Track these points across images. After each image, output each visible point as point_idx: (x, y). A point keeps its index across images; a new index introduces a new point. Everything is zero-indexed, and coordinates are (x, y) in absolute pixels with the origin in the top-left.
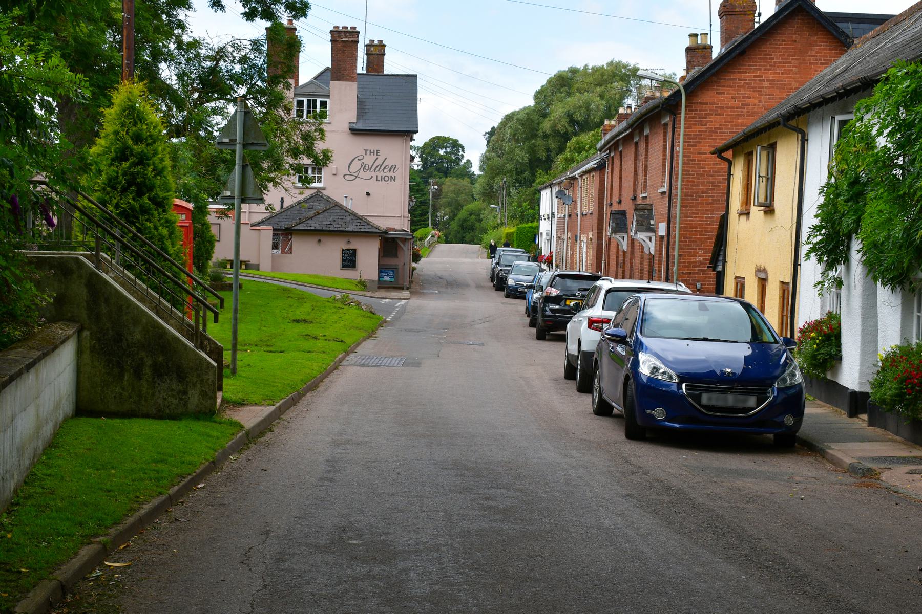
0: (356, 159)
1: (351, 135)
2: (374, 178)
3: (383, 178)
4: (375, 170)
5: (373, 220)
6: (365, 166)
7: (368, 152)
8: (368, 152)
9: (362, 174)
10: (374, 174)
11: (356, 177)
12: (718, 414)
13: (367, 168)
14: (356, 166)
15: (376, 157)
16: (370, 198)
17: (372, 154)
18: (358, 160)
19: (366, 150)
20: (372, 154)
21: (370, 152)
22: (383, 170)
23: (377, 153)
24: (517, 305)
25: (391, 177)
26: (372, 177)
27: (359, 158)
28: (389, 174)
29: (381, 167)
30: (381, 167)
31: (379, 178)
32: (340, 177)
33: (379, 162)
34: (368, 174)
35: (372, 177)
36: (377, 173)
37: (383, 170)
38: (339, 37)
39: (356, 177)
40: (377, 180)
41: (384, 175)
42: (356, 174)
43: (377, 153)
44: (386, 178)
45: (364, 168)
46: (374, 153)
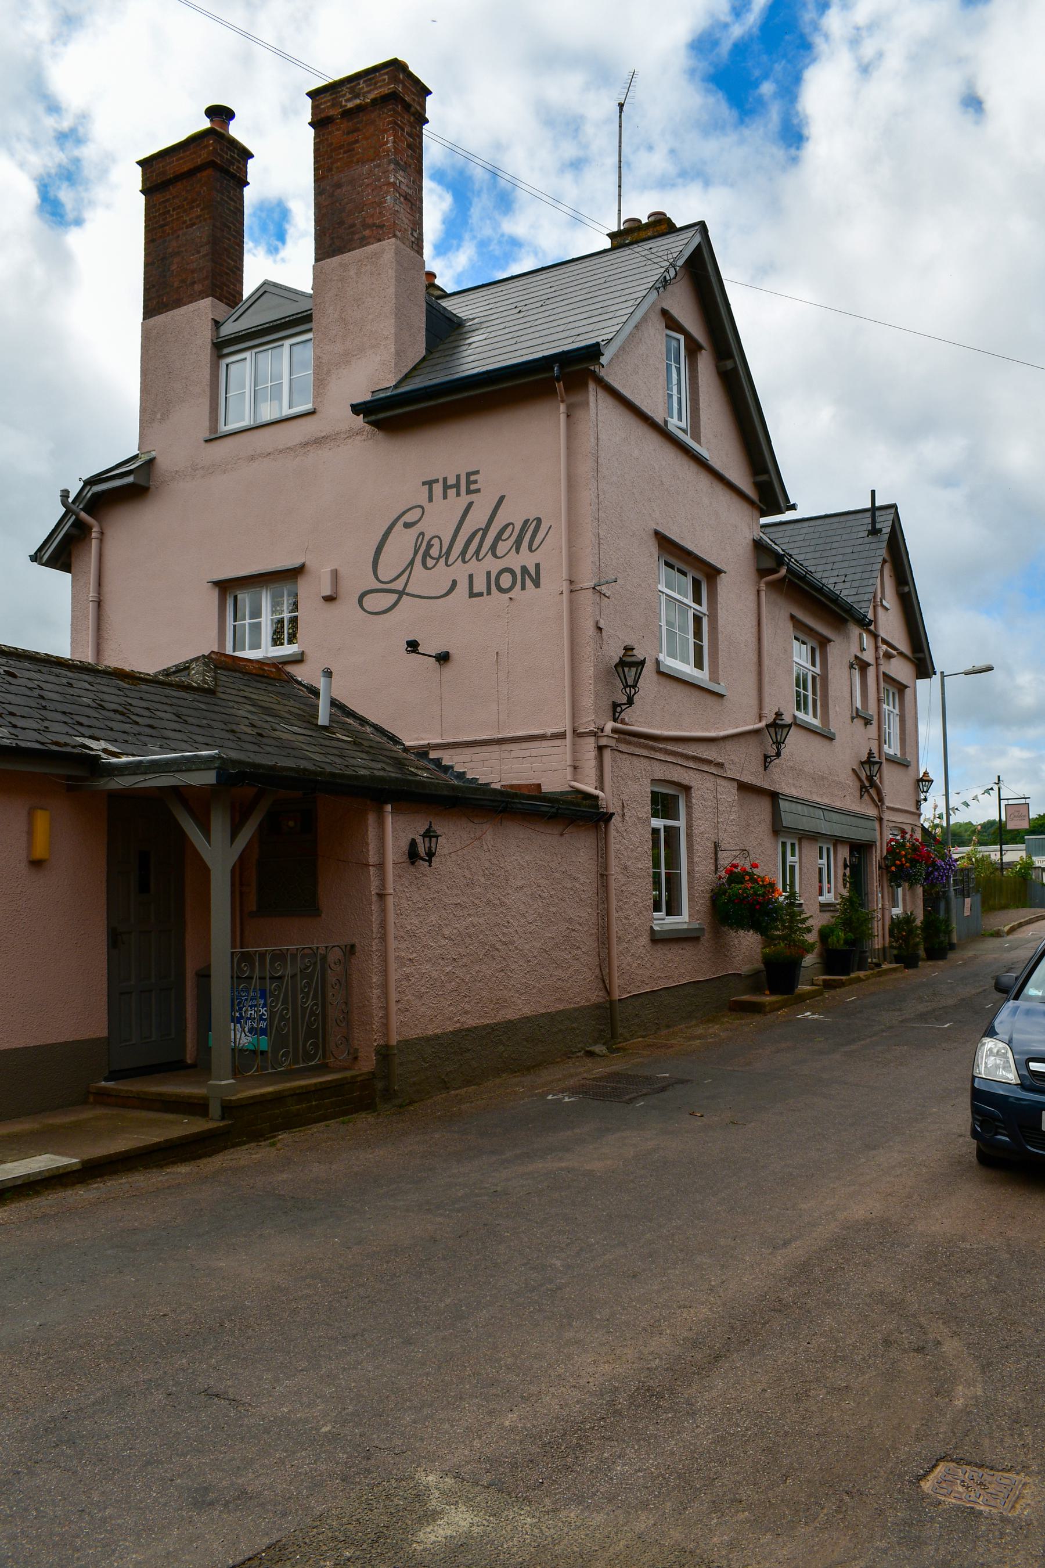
0: (400, 523)
1: (380, 435)
2: (463, 587)
3: (493, 583)
4: (463, 553)
5: (455, 760)
6: (429, 546)
7: (438, 489)
8: (438, 489)
9: (421, 580)
10: (460, 571)
11: (401, 593)
12: (801, 584)
13: (434, 552)
14: (402, 543)
15: (465, 499)
16: (450, 670)
17: (452, 492)
18: (407, 525)
19: (430, 484)
20: (452, 492)
21: (446, 487)
22: (493, 548)
23: (468, 483)
24: (304, 1130)
25: (524, 570)
26: (454, 583)
27: (409, 518)
28: (515, 561)
29: (1020, 816)
30: (1020, 816)
31: (480, 585)
32: (347, 606)
33: (477, 518)
34: (437, 578)
35: (454, 583)
36: (473, 566)
37: (493, 548)
38: (335, 104)
39: (401, 593)
40: (472, 595)
41: (494, 565)
42: (398, 585)
43: (468, 483)
44: (506, 581)
45: (427, 554)
46: (457, 486)
